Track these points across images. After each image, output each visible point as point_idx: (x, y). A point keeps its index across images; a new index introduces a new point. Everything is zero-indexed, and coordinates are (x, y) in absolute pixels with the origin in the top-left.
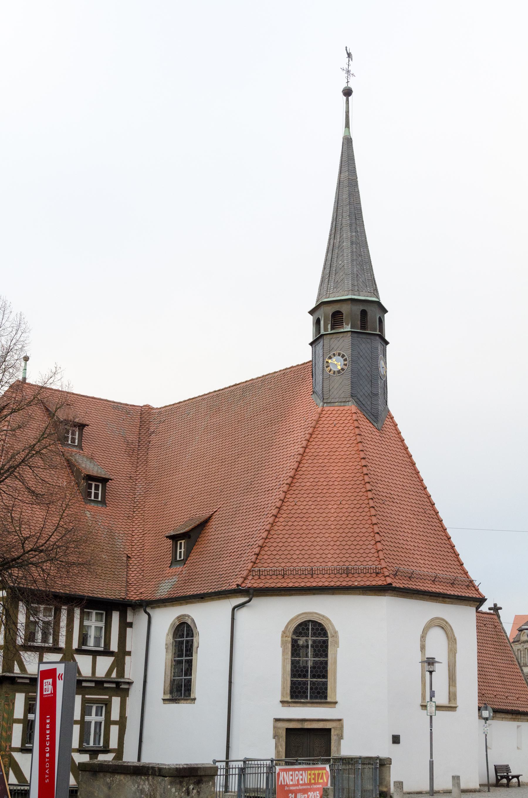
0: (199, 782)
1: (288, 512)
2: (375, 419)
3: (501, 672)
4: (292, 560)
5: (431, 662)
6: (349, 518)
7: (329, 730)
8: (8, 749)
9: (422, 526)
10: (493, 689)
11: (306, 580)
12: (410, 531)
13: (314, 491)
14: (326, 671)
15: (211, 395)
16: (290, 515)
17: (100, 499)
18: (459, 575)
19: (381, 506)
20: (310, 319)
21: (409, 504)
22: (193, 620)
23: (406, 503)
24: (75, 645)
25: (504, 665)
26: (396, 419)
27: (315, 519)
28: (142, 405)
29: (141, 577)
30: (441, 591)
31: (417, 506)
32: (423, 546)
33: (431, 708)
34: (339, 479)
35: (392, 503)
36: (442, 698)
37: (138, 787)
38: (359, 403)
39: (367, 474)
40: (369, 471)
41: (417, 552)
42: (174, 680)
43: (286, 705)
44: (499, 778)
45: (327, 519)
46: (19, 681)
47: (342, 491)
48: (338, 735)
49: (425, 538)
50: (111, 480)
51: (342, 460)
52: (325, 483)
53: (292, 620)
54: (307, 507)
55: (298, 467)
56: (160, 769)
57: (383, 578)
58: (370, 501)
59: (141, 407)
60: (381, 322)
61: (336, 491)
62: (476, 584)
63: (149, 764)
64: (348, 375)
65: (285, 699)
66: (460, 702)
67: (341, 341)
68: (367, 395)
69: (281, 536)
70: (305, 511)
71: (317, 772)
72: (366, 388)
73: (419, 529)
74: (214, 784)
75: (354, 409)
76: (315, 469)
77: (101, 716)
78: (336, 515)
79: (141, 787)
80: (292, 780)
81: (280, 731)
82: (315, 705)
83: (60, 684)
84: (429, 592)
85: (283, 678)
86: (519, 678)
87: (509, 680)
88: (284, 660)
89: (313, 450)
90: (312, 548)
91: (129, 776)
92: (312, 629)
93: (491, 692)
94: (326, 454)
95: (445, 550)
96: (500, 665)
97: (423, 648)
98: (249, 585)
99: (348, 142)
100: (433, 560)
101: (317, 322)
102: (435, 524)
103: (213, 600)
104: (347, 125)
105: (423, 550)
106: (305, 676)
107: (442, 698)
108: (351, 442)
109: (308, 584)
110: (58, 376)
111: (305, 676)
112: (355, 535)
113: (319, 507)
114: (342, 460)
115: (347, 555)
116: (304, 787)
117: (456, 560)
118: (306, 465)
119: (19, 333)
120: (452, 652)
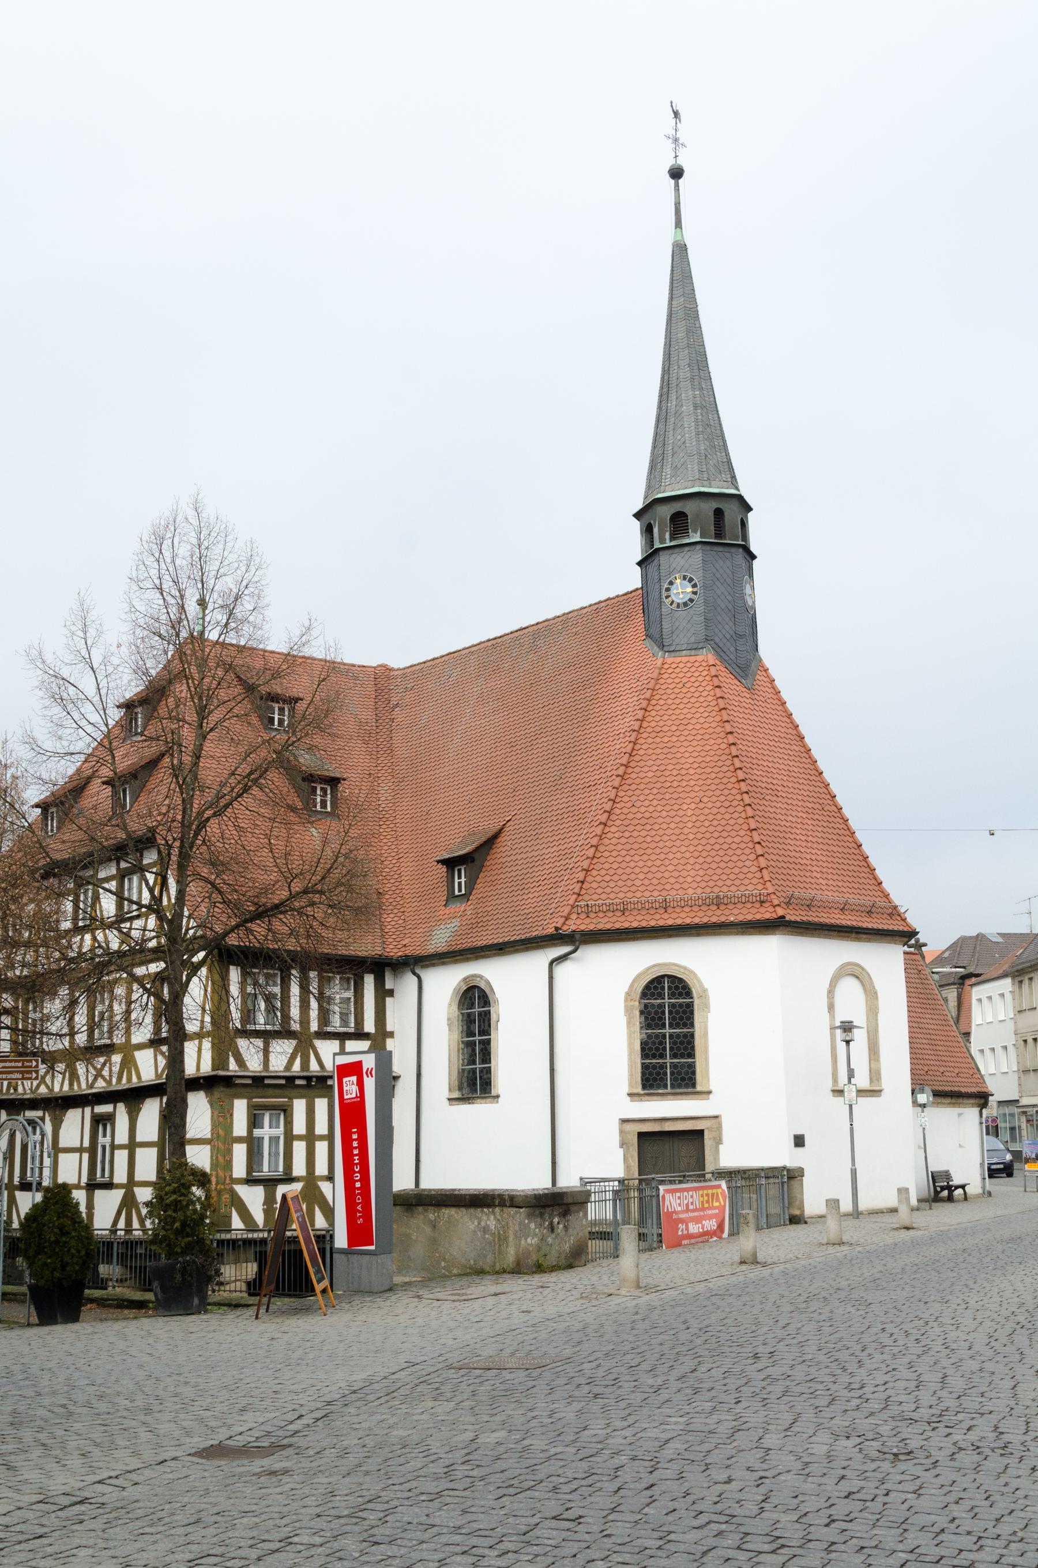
0: (565, 1214)
1: (623, 817)
2: (742, 674)
3: (932, 1037)
4: (634, 889)
5: (847, 1027)
6: (715, 823)
7: (701, 1133)
8: (228, 1181)
9: (820, 829)
10: (922, 1062)
11: (657, 916)
12: (803, 838)
13: (659, 785)
14: (693, 1048)
15: (483, 645)
16: (626, 822)
17: (329, 809)
18: (877, 900)
19: (761, 802)
20: (636, 525)
21: (800, 798)
22: (488, 983)
23: (795, 797)
24: (314, 1027)
25: (935, 1027)
26: (772, 672)
27: (665, 826)
28: (375, 665)
29: (401, 922)
30: (855, 924)
31: (811, 800)
32: (824, 859)
33: (851, 1093)
34: (696, 765)
35: (775, 798)
36: (862, 1080)
37: (479, 1224)
38: (719, 650)
39: (737, 756)
40: (740, 752)
41: (815, 868)
42: (463, 1070)
43: (636, 1098)
44: (939, 1189)
45: (681, 825)
46: (238, 1081)
47: (701, 782)
48: (714, 1139)
49: (825, 847)
50: (344, 780)
51: (699, 737)
52: (675, 772)
53: (639, 976)
54: (651, 809)
55: (633, 749)
56: (512, 1198)
57: (771, 909)
58: (745, 795)
59: (375, 668)
60: (744, 524)
61: (692, 783)
62: (902, 910)
63: (493, 1190)
64: (699, 607)
65: (635, 1091)
66: (886, 1083)
67: (686, 557)
68: (728, 636)
69: (615, 853)
70: (647, 815)
71: (710, 1192)
72: (727, 627)
73: (816, 833)
74: (586, 1214)
75: (712, 659)
76: (658, 751)
77: (278, 1127)
78: (694, 818)
79: (483, 1224)
80: (680, 1205)
81: (629, 1136)
82: (679, 1097)
83: (370, 1083)
84: (838, 926)
85: (630, 1059)
86: (957, 1044)
87: (943, 1048)
88: (630, 1034)
89: (653, 724)
90: (663, 869)
91: (463, 1210)
92: (670, 988)
93: (920, 1067)
94: (674, 728)
95: (855, 863)
96: (930, 1026)
97: (831, 1007)
98: (573, 927)
99: (680, 251)
100: (840, 878)
101: (648, 530)
102: (838, 825)
103: (517, 951)
104: (678, 224)
105: (825, 865)
106: (662, 1056)
107: (862, 1080)
108: (710, 709)
109: (661, 923)
110: (315, 633)
111: (662, 1056)
112: (725, 846)
113: (668, 808)
114: (699, 737)
115: (716, 878)
116: (696, 1214)
117: (871, 877)
118: (645, 746)
119: (253, 569)
120: (873, 1011)
